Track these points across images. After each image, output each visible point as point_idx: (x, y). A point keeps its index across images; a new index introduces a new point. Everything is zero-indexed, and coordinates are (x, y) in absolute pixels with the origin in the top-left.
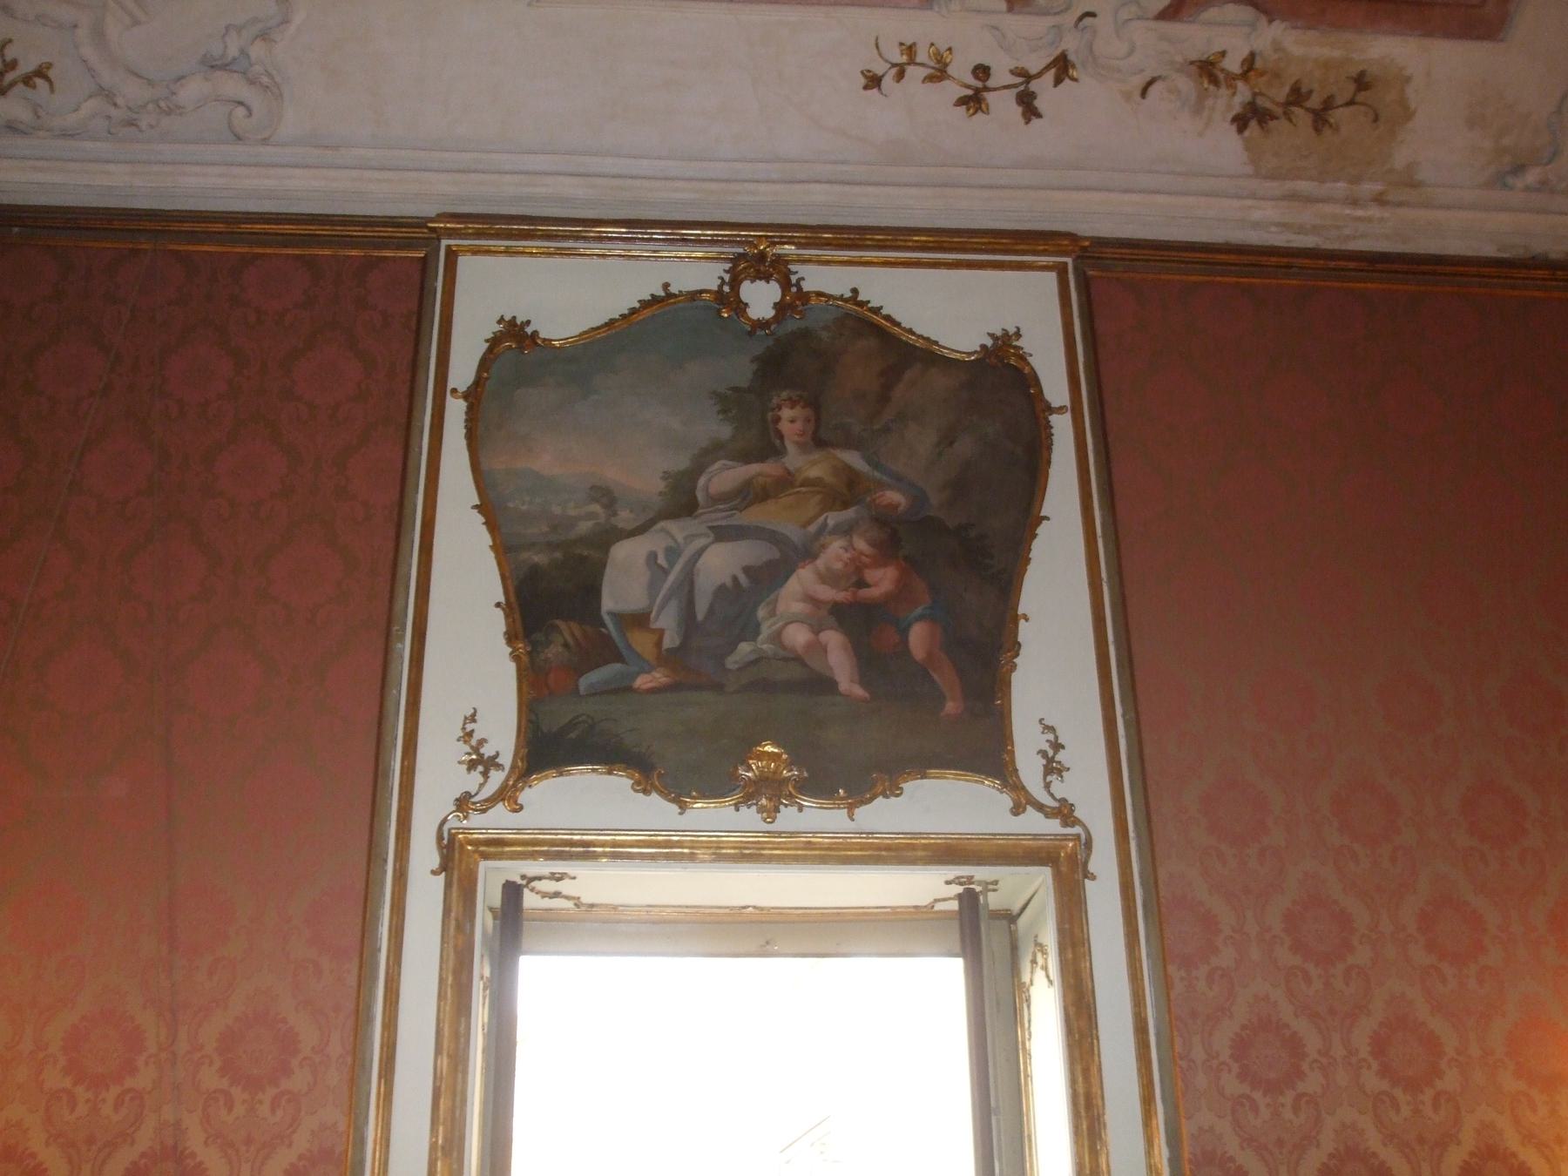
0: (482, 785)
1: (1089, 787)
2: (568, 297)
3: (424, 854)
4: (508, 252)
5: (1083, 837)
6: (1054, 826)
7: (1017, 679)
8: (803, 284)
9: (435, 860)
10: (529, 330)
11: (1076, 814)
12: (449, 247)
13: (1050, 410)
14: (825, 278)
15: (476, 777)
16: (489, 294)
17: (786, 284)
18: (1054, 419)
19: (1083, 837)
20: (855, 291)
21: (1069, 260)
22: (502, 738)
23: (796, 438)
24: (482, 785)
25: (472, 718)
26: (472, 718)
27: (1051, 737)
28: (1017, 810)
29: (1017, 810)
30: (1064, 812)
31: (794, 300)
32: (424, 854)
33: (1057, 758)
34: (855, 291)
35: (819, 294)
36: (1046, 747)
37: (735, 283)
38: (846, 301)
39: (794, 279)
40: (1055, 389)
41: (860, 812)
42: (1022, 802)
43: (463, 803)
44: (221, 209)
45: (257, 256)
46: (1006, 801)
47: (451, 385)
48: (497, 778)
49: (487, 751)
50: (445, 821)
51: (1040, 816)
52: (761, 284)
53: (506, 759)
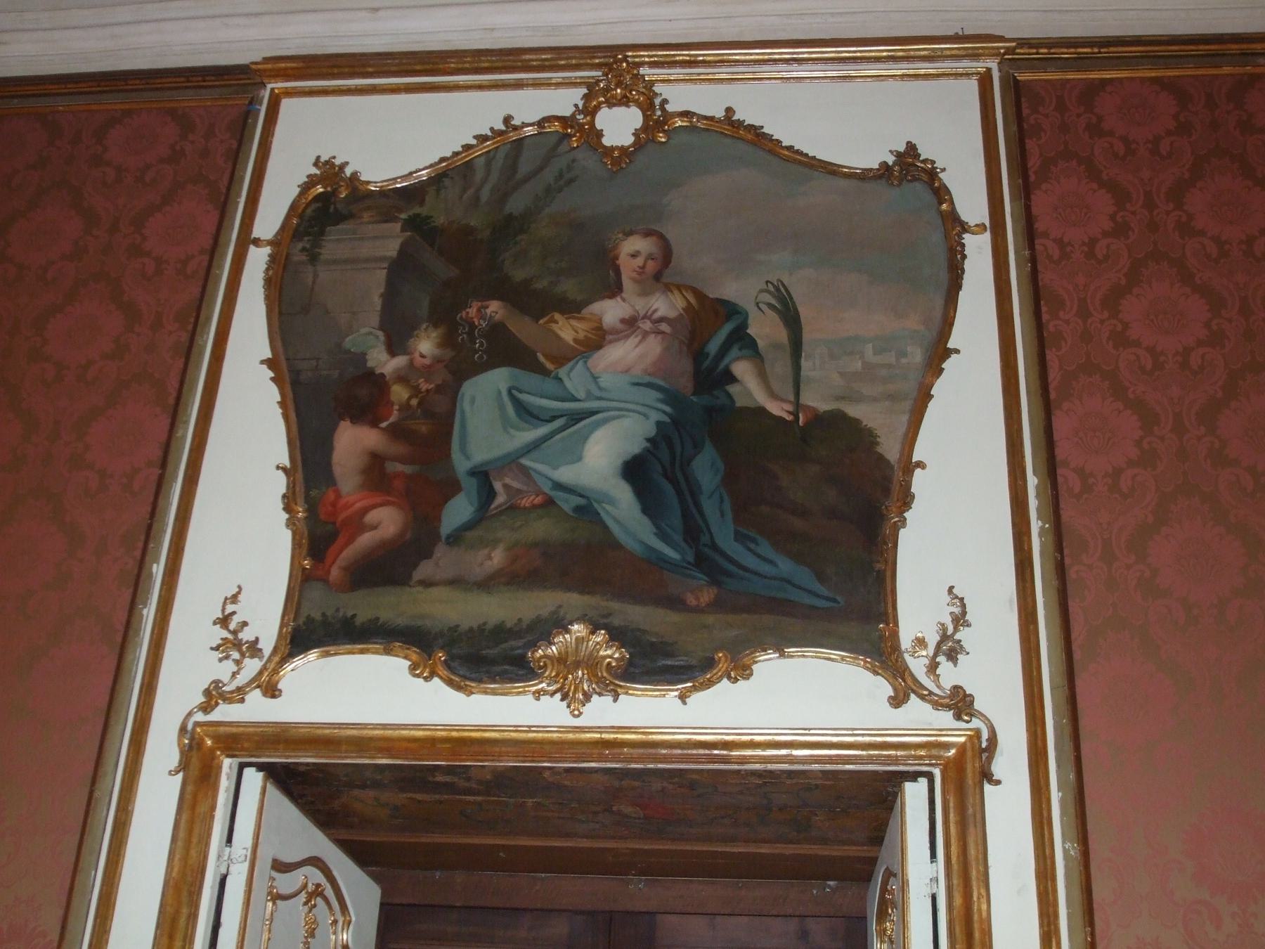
0: (234, 675)
1: (993, 673)
2: (397, 139)
3: (162, 751)
4: (537, 84)
5: (985, 735)
6: (945, 718)
7: (906, 539)
8: (667, 107)
9: (174, 758)
10: (348, 171)
11: (977, 706)
12: (272, 90)
13: (964, 228)
14: (685, 96)
15: (230, 666)
16: (306, 138)
17: (647, 107)
18: (968, 238)
19: (985, 735)
20: (729, 110)
21: (993, 65)
22: (265, 619)
23: (634, 275)
24: (234, 675)
25: (234, 599)
26: (234, 599)
27: (957, 610)
28: (897, 701)
29: (897, 701)
30: (960, 703)
31: (656, 120)
32: (162, 751)
33: (957, 637)
34: (729, 110)
35: (686, 114)
36: (948, 621)
37: (591, 112)
38: (719, 121)
39: (657, 101)
40: (971, 202)
41: (697, 698)
42: (904, 688)
43: (214, 695)
44: (74, 71)
45: (1104, 82)
46: (885, 689)
47: (987, 237)
48: (252, 666)
49: (246, 635)
50: (190, 714)
51: (928, 707)
52: (620, 111)
53: (267, 645)
